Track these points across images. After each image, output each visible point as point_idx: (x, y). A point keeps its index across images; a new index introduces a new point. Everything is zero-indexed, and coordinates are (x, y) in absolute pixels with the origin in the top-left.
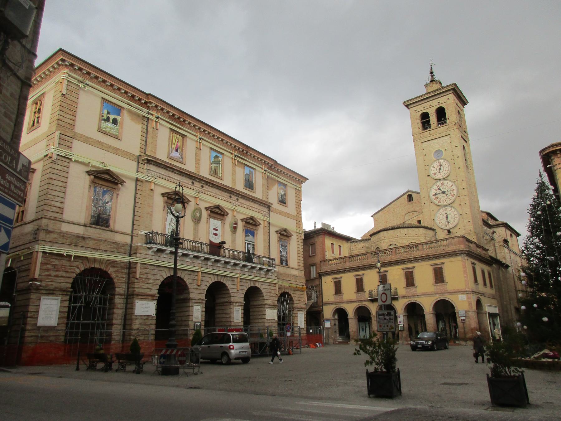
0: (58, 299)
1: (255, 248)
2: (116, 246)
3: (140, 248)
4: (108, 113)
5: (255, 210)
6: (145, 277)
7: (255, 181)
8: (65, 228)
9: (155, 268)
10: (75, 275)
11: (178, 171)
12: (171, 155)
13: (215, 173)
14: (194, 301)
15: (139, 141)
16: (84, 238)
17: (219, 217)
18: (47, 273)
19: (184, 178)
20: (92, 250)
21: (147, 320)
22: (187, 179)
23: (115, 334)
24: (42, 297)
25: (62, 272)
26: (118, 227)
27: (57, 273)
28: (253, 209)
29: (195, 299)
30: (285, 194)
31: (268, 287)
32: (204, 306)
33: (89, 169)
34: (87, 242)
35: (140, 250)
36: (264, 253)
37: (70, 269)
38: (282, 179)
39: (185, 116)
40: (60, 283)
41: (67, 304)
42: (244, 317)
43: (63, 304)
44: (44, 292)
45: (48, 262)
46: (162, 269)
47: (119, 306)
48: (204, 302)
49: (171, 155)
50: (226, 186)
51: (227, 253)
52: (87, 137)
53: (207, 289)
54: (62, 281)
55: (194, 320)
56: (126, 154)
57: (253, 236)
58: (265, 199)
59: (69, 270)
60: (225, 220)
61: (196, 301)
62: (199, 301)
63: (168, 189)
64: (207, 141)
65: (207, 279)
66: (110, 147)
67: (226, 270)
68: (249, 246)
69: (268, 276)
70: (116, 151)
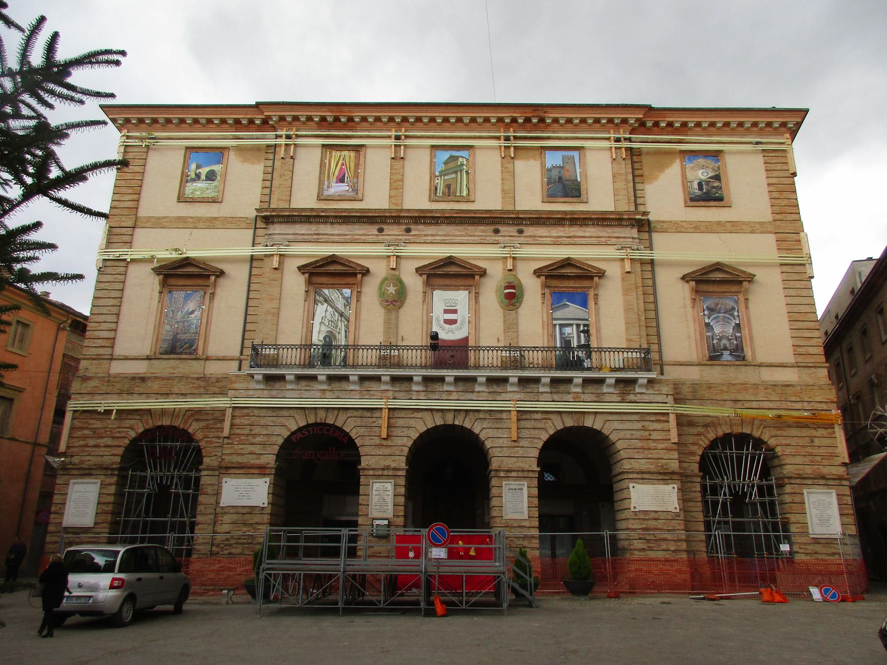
0: (95, 483)
1: (593, 331)
2: (203, 384)
4: (198, 167)
5: (583, 241)
6: (246, 432)
7: (584, 174)
8: (117, 368)
9: (270, 413)
10: (127, 442)
11: (336, 217)
12: (326, 193)
13: (449, 192)
14: (371, 472)
16: (143, 379)
17: (199, 282)
18: (82, 443)
19: (357, 227)
20: (159, 396)
21: (248, 516)
22: (366, 226)
23: (200, 541)
25: (105, 439)
27: (99, 441)
28: (583, 241)
29: (374, 469)
30: (717, 178)
31: (638, 426)
33: (155, 265)
34: (149, 384)
35: (235, 382)
36: (628, 340)
37: (119, 432)
38: (697, 143)
39: (346, 109)
40: (102, 456)
41: (112, 489)
42: (540, 506)
43: (105, 491)
44: (75, 472)
45: (85, 426)
46: (285, 413)
47: (210, 490)
48: (403, 473)
49: (326, 193)
51: (486, 358)
52: (159, 218)
53: (410, 444)
54: (106, 453)
55: (374, 513)
56: (753, 228)
57: (584, 304)
58: (511, 208)
59: (118, 435)
60: (477, 286)
61: (380, 473)
62: (386, 473)
63: (307, 256)
64: (306, 136)
65: (412, 423)
66: (199, 219)
67: (474, 396)
68: (568, 330)
69: (632, 397)
70: (735, 227)
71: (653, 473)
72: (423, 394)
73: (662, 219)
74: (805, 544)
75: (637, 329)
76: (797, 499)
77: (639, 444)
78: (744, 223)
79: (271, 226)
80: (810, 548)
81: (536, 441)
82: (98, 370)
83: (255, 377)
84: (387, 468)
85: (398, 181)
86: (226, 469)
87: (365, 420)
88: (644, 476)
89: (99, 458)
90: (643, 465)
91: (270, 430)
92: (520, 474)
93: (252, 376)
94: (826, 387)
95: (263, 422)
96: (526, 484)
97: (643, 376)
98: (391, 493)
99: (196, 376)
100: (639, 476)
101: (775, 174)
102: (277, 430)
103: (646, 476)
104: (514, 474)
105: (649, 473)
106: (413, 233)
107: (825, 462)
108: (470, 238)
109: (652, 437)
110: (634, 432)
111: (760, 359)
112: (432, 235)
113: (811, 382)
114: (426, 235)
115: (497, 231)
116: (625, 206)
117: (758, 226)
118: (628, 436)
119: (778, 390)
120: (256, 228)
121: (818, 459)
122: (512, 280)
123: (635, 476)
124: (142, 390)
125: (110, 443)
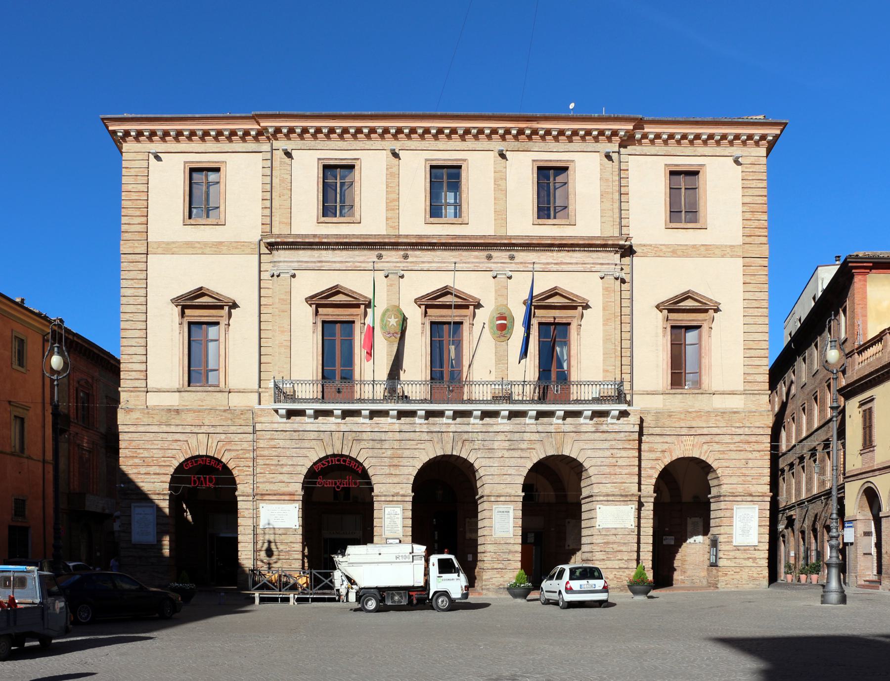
2: (230, 416)
3: (260, 413)
5: (570, 268)
6: (275, 462)
8: (153, 400)
14: (383, 499)
15: (259, 211)
16: (177, 411)
24: (133, 505)
26: (233, 383)
29: (385, 496)
31: (608, 453)
32: (520, 505)
34: (183, 416)
35: (261, 416)
36: (605, 371)
37: (165, 461)
47: (246, 513)
48: (410, 499)
50: (476, 237)
51: (478, 392)
52: (168, 243)
53: (415, 473)
56: (725, 251)
58: (501, 232)
59: (163, 464)
61: (391, 499)
62: (395, 499)
65: (416, 453)
66: (205, 244)
70: (707, 251)
71: (617, 495)
72: (425, 426)
73: (643, 243)
74: (728, 551)
75: (613, 359)
76: (728, 514)
77: (607, 470)
78: (717, 247)
79: (274, 252)
80: (732, 554)
81: (521, 469)
82: (138, 403)
83: (280, 411)
84: (397, 494)
85: (394, 200)
86: (258, 496)
87: (376, 451)
88: (610, 499)
89: (151, 485)
90: (608, 488)
91: (295, 461)
92: (508, 499)
93: (276, 411)
94: (765, 413)
95: (288, 453)
96: (512, 507)
97: (615, 408)
98: (400, 516)
99: (222, 408)
100: (605, 498)
101: (751, 192)
102: (301, 461)
103: (611, 498)
104: (502, 499)
105: (613, 495)
106: (516, 260)
107: (754, 482)
108: (464, 265)
109: (618, 464)
110: (603, 460)
111: (714, 388)
112: (429, 262)
113: (754, 408)
114: (423, 262)
115: (489, 257)
116: (611, 232)
117: (728, 250)
118: (599, 464)
119: (726, 417)
120: (260, 254)
121: (749, 478)
122: (503, 311)
123: (602, 498)
124: (178, 422)
125: (158, 471)
